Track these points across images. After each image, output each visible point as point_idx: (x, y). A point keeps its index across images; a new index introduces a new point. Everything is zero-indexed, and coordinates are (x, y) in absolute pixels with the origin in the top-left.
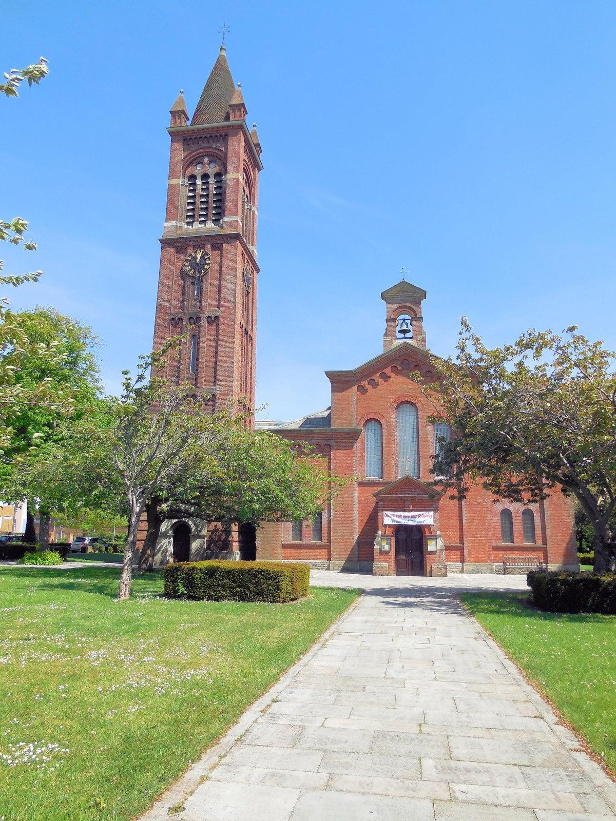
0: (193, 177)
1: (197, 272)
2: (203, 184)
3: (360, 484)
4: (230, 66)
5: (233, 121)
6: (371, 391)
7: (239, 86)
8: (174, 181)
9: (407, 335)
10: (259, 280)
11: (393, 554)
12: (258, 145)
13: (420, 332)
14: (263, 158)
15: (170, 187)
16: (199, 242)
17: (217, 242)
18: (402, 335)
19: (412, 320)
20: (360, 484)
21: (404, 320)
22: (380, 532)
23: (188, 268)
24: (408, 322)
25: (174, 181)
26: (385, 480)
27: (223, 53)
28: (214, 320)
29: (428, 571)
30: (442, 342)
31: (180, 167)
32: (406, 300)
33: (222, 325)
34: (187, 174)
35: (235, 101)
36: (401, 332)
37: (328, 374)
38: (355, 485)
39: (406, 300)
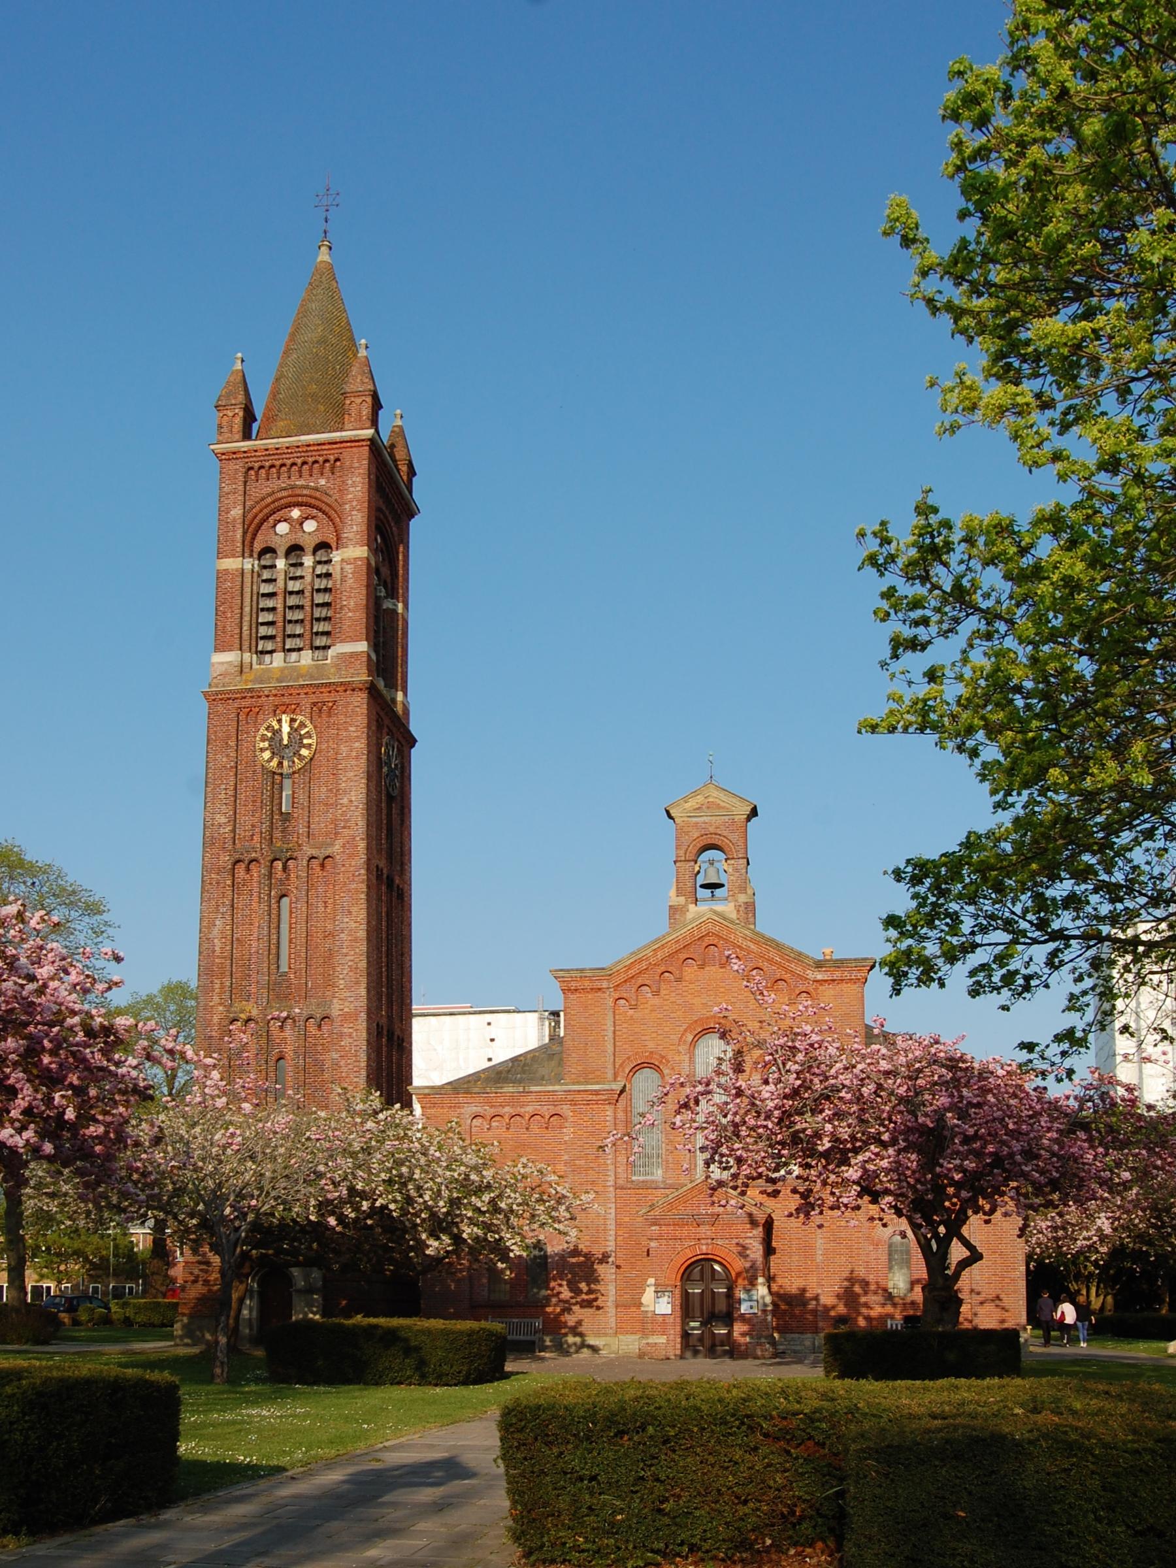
1: (285, 763)
34: (258, 547)
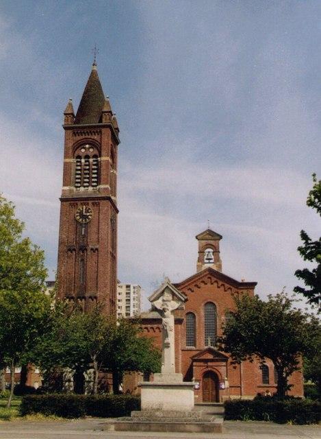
0: (79, 157)
2: (86, 161)
3: (182, 350)
4: (107, 94)
5: (105, 122)
6: (274, 294)
7: (119, 301)
8: (68, 160)
9: (211, 261)
10: (119, 148)
11: (201, 390)
12: (117, 129)
13: (217, 260)
14: (121, 136)
15: (65, 164)
16: (85, 200)
17: (96, 201)
18: (208, 261)
19: (213, 252)
20: (182, 350)
21: (209, 252)
22: (194, 378)
23: (78, 217)
24: (211, 253)
25: (68, 160)
26: (197, 348)
27: (95, 68)
28: (95, 250)
29: (220, 400)
30: (232, 268)
31: (71, 151)
32: (210, 240)
33: (101, 253)
34: (76, 155)
35: (105, 109)
36: (207, 259)
37: (302, 232)
38: (180, 352)
39: (210, 240)
